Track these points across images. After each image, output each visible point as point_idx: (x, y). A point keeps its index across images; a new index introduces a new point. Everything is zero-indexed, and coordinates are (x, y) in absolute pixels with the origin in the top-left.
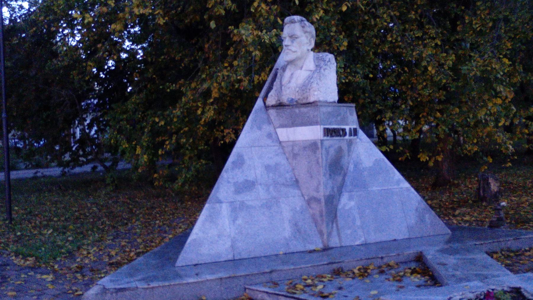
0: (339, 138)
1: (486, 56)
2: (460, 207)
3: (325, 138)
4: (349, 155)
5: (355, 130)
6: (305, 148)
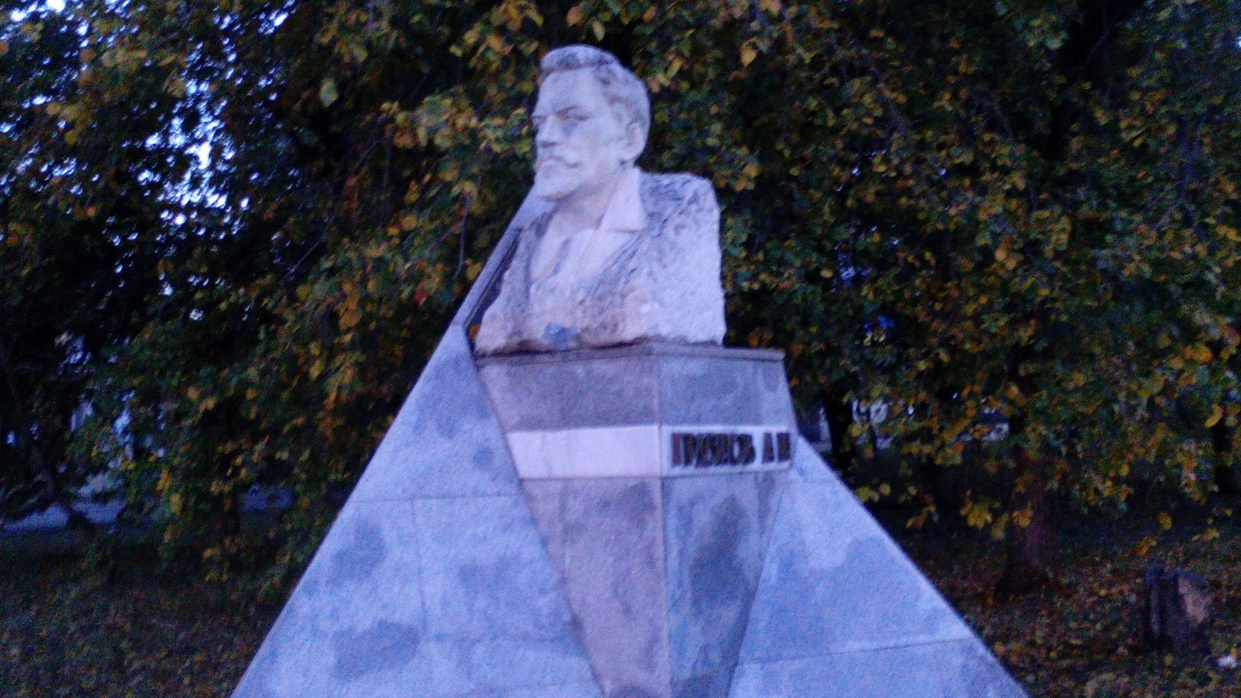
0: (726, 469)
1: (1165, 219)
2: (1095, 667)
3: (678, 470)
4: (762, 530)
5: (784, 439)
6: (605, 505)
